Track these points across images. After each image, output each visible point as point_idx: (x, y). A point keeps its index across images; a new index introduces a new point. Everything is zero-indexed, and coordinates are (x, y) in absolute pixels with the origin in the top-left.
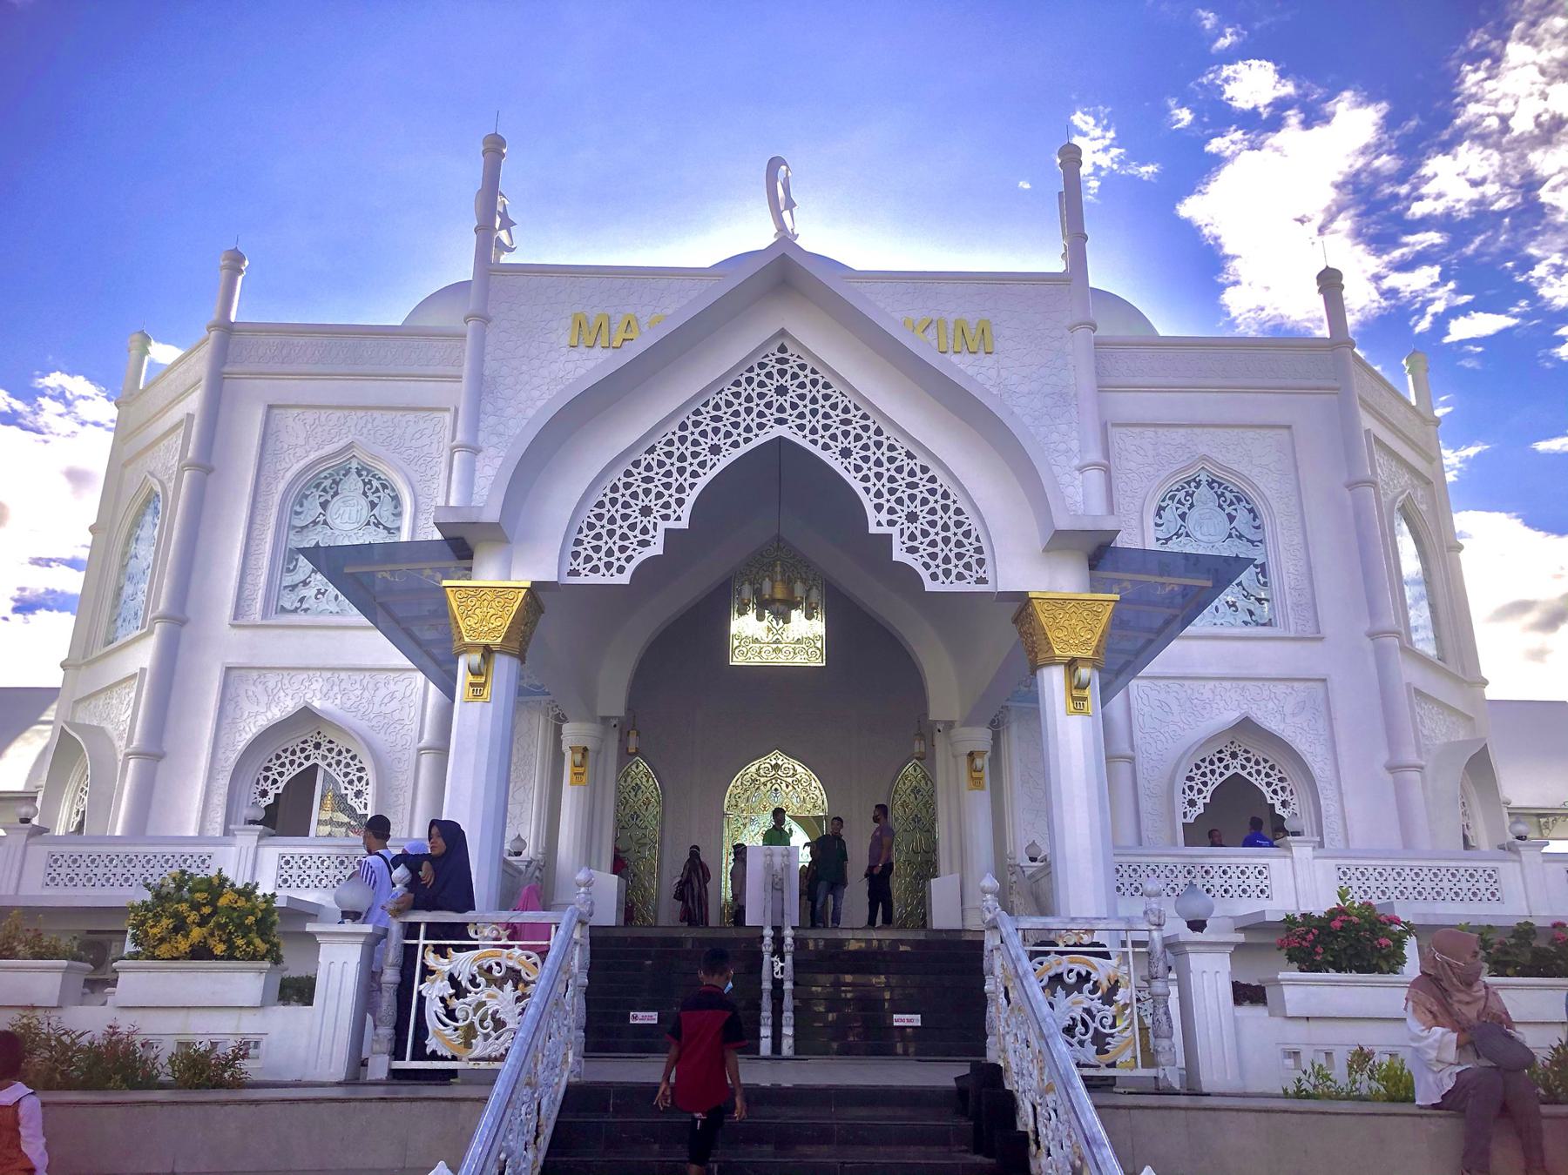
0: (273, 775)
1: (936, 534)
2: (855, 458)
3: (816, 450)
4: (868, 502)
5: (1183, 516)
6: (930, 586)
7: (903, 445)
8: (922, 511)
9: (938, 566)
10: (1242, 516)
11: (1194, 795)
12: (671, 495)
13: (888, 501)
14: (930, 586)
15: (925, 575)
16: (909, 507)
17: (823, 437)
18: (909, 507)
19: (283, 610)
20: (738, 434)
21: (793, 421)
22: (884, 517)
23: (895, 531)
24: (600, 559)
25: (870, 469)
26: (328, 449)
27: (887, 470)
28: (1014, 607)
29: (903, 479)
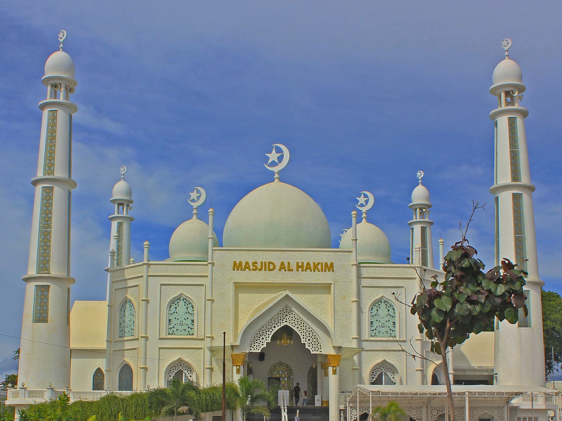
0: (171, 372)
1: (313, 343)
2: (299, 329)
3: (292, 327)
4: (302, 337)
5: (377, 310)
6: (312, 353)
7: (308, 327)
8: (311, 339)
9: (313, 349)
10: (391, 310)
11: (373, 376)
12: (267, 336)
13: (305, 337)
14: (312, 353)
15: (311, 350)
16: (309, 338)
17: (294, 325)
18: (309, 338)
19: (169, 334)
20: (279, 324)
21: (289, 322)
22: (304, 340)
23: (306, 342)
24: (255, 347)
25: (302, 331)
26: (177, 295)
27: (305, 331)
28: (312, 402)
29: (308, 333)
